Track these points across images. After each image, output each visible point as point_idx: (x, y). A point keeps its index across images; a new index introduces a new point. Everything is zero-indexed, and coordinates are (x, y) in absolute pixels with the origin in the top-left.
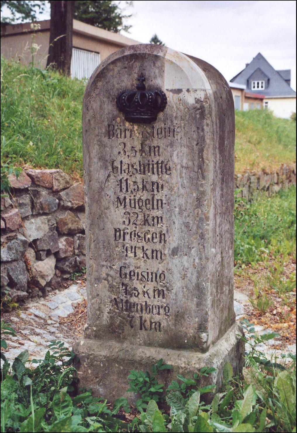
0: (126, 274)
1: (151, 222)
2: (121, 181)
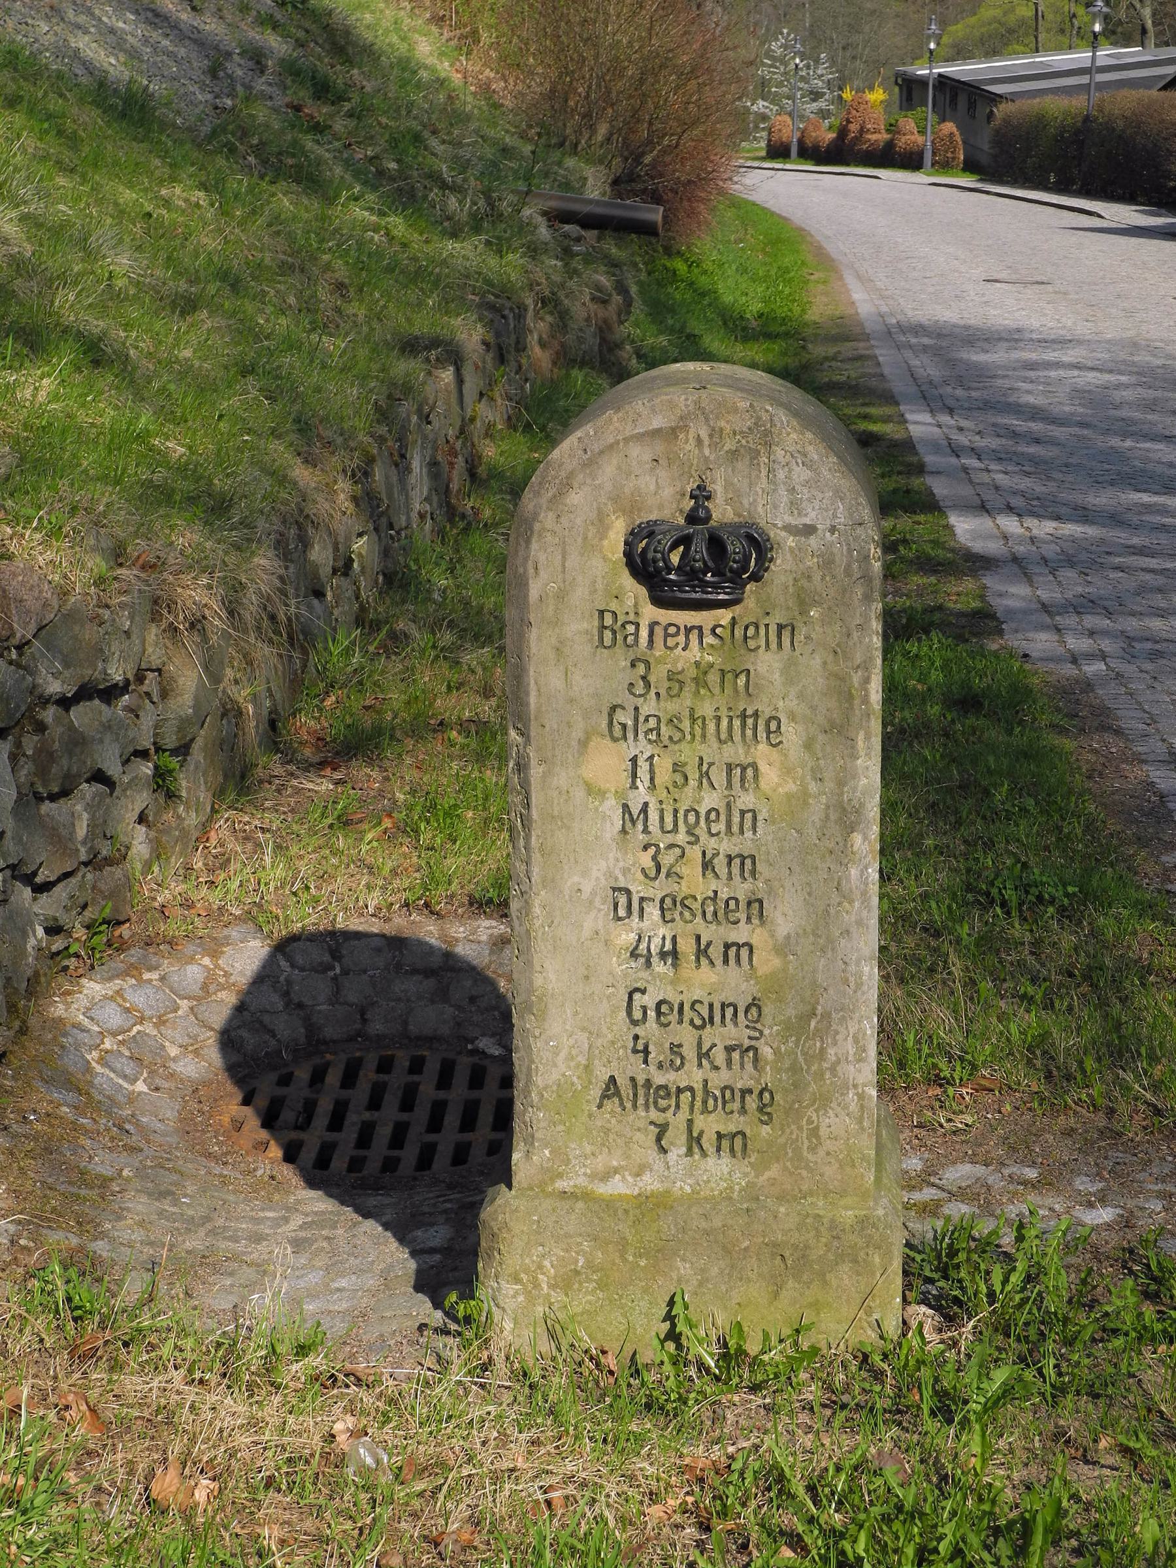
0: (644, 1009)
1: (722, 870)
2: (634, 760)
